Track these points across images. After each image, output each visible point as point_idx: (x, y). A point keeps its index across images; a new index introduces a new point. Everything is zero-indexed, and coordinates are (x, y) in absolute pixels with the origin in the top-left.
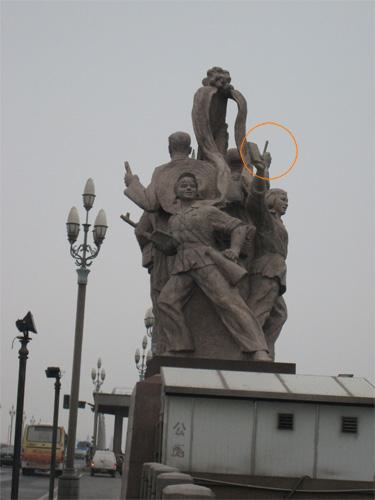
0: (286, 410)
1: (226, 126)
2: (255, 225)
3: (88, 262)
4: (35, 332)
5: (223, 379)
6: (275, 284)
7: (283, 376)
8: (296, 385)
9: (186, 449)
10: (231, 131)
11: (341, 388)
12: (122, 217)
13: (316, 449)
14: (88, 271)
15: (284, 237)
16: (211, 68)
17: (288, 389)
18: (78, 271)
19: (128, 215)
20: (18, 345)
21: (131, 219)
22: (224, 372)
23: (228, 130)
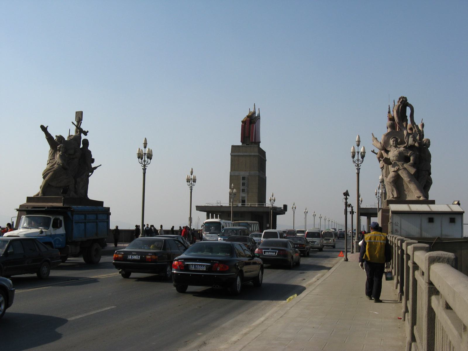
0: (430, 216)
1: (407, 116)
3: (359, 165)
4: (349, 196)
5: (410, 208)
7: (430, 205)
8: (434, 208)
9: (399, 230)
10: (409, 118)
12: (372, 151)
13: (441, 228)
15: (429, 156)
17: (431, 210)
18: (357, 168)
19: (374, 150)
20: (344, 201)
21: (375, 151)
22: (410, 205)
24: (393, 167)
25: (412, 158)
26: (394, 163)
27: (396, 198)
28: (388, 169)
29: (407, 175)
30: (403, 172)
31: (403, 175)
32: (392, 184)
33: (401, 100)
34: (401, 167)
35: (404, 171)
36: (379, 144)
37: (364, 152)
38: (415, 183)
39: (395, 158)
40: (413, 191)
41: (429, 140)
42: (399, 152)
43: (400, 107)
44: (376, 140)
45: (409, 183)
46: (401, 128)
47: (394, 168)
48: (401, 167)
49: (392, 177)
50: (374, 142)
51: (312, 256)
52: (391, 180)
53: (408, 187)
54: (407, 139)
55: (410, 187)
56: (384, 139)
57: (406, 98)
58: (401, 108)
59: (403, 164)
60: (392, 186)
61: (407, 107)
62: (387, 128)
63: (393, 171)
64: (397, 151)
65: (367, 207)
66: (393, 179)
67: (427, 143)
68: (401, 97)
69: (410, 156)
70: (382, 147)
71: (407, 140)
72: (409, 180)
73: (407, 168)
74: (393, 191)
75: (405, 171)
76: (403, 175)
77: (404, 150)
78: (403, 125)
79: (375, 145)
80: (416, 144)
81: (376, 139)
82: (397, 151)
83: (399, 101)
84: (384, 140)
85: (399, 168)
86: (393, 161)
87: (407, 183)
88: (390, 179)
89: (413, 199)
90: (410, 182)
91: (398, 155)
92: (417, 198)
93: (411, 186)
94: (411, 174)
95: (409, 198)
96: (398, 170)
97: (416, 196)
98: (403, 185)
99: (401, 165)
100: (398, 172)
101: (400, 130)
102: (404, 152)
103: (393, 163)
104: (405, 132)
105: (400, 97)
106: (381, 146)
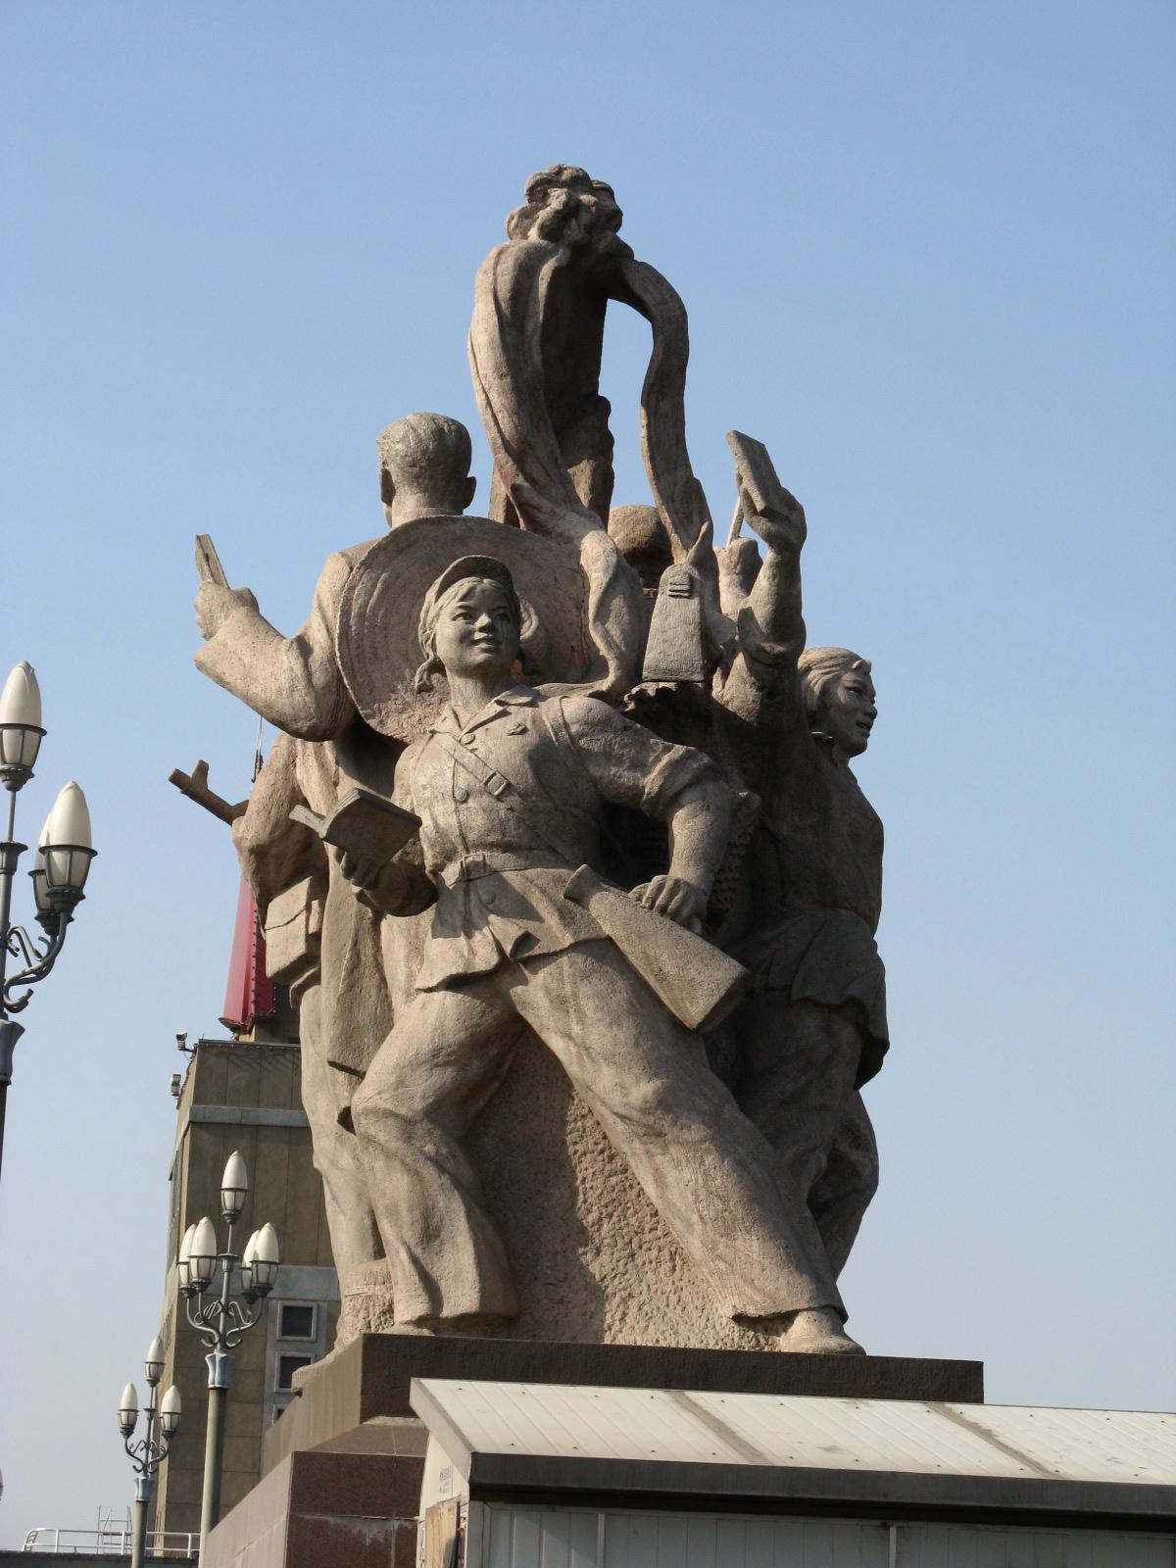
1: (604, 407)
2: (752, 787)
6: (847, 1034)
10: (628, 426)
11: (433, 1391)
12: (178, 779)
14: (16, 1031)
15: (869, 834)
16: (879, 704)
19: (203, 769)
21: (215, 785)
23: (614, 424)
24: (453, 933)
25: (685, 829)
26: (467, 875)
27: (463, 1321)
28: (369, 983)
29: (625, 1032)
30: (585, 989)
31: (576, 1029)
32: (429, 1148)
33: (557, 199)
34: (554, 932)
35: (586, 977)
36: (288, 662)
37: (81, 850)
38: (724, 1142)
39: (477, 817)
40: (695, 1245)
41: (864, 669)
42: (531, 738)
43: (547, 270)
44: (239, 614)
45: (654, 1134)
46: (545, 504)
47: (462, 940)
48: (554, 932)
49: (436, 1052)
50: (222, 634)
51: (597, 1544)
52: (424, 1087)
53: (631, 1184)
54: (614, 628)
55: (651, 1190)
56: (348, 601)
57: (606, 191)
58: (552, 286)
59: (578, 896)
60: (430, 1172)
61: (613, 305)
62: (388, 493)
63: (454, 983)
64: (509, 724)
65: (38, 1547)
66: (447, 1075)
67: (841, 694)
68: (560, 171)
69: (668, 800)
70: (318, 695)
71: (615, 632)
72: (644, 1090)
73: (624, 946)
74: (430, 1233)
75: (598, 984)
76: (576, 1029)
77: (594, 725)
78: (568, 484)
79: (233, 676)
80: (734, 689)
81: (248, 601)
82: (509, 724)
83: (527, 215)
84: (345, 613)
85: (525, 940)
86: (449, 856)
87: (618, 1130)
88: (400, 1083)
89: (694, 1343)
90: (666, 1124)
91: (524, 778)
92: (736, 1331)
93: (672, 1176)
94: (677, 1025)
95: (626, 1330)
96: (520, 958)
97: (725, 1310)
98: (560, 1168)
99: (553, 902)
100: (517, 991)
101: (531, 520)
102: (593, 744)
103: (451, 874)
104: (596, 555)
105: (546, 168)
106: (301, 685)
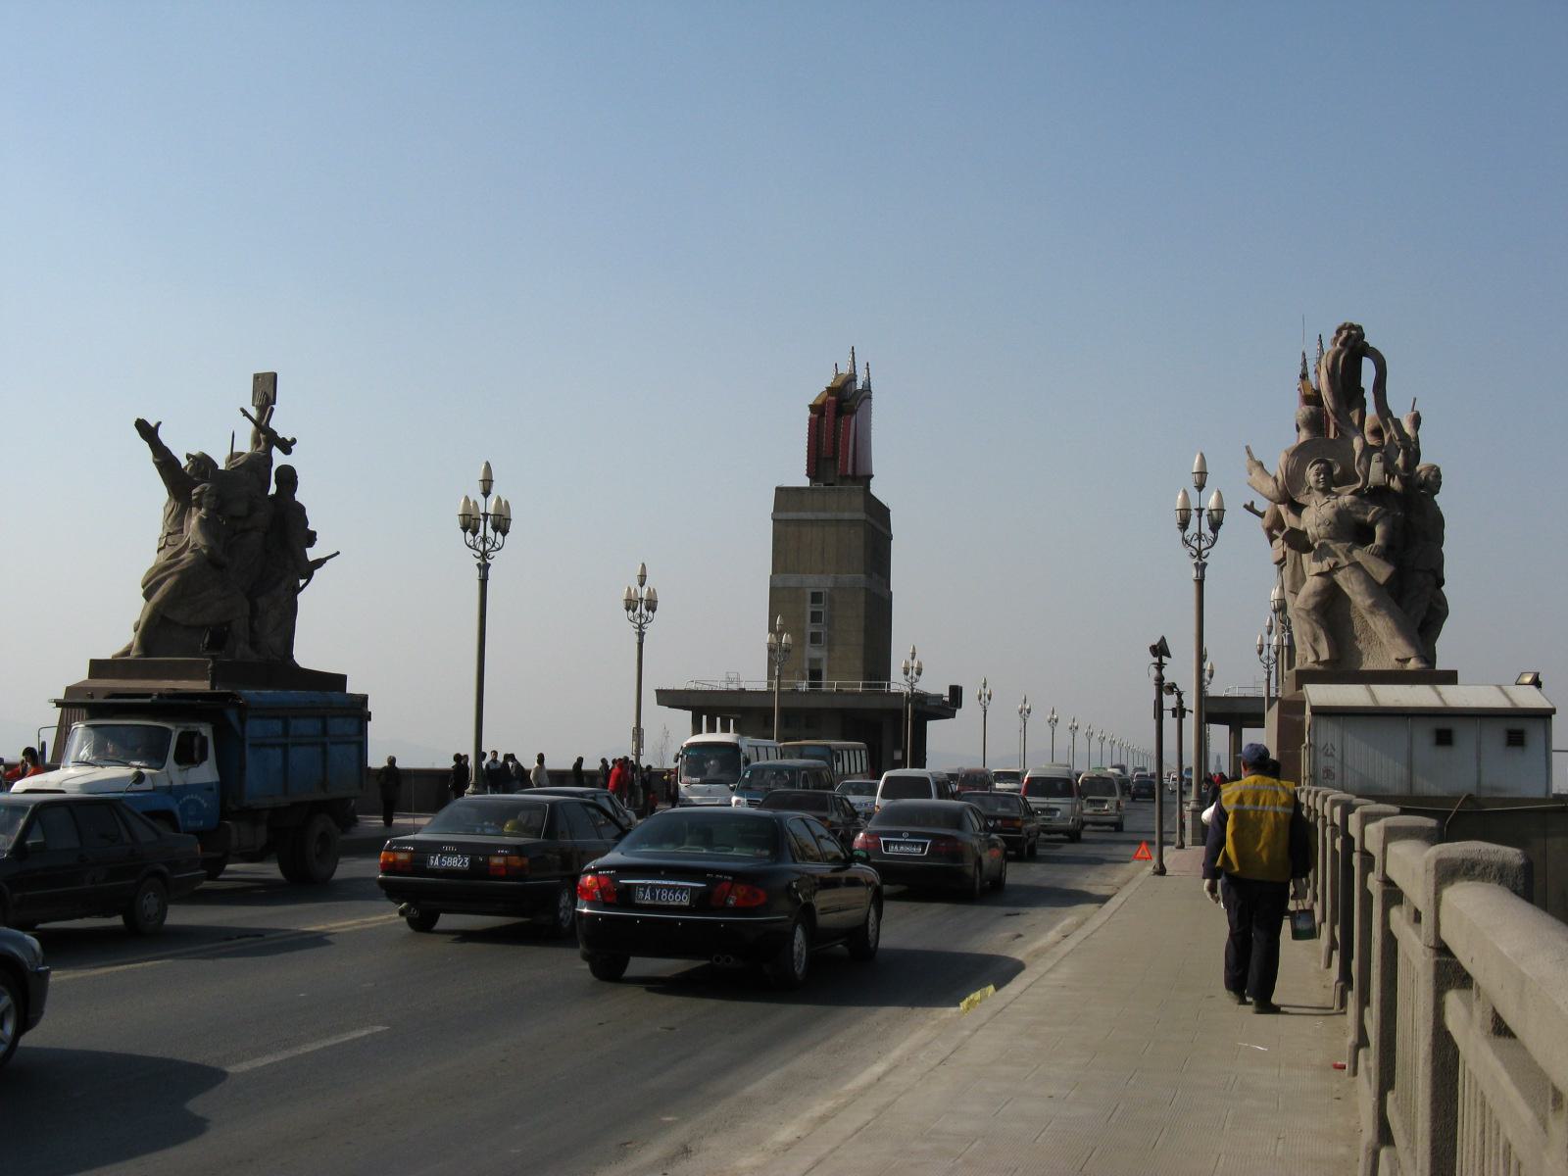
0: (1441, 724)
1: (1363, 390)
3: (1204, 553)
4: (1169, 656)
5: (1373, 695)
7: (1441, 688)
8: (1455, 696)
9: (1336, 771)
10: (1369, 396)
12: (1246, 506)
13: (1478, 765)
15: (1439, 521)
17: (1445, 703)
18: (1196, 564)
19: (1252, 503)
20: (1154, 672)
21: (1256, 507)
22: (1373, 687)
24: (1317, 561)
25: (1379, 530)
26: (1320, 545)
27: (1325, 662)
28: (1299, 567)
29: (1363, 587)
30: (1352, 576)
31: (1350, 586)
32: (1314, 618)
33: (1345, 333)
34: (1344, 561)
35: (1353, 572)
36: (1271, 483)
37: (1221, 510)
38: (1391, 614)
39: (1322, 531)
40: (1385, 641)
41: (1438, 470)
42: (1336, 509)
43: (1342, 357)
44: (1258, 469)
45: (1372, 613)
46: (1344, 428)
47: (1319, 563)
48: (1344, 561)
49: (1315, 592)
50: (1254, 475)
51: (1044, 856)
52: (1312, 602)
53: (1367, 625)
54: (1362, 467)
55: (1373, 627)
56: (1287, 466)
57: (1359, 328)
58: (1343, 362)
59: (1350, 551)
60: (1314, 624)
61: (1364, 358)
62: (1298, 430)
63: (1318, 574)
64: (1330, 505)
65: (1229, 694)
66: (1318, 599)
67: (1431, 478)
68: (1345, 324)
69: (1374, 522)
70: (1280, 493)
71: (1363, 469)
72: (1369, 602)
73: (1363, 564)
74: (1316, 639)
75: (1356, 575)
76: (1350, 586)
77: (1353, 503)
78: (1351, 420)
79: (1257, 487)
80: (1395, 484)
81: (1261, 465)
82: (1330, 505)
83: (1336, 339)
84: (1287, 469)
85: (1336, 564)
86: (1315, 540)
87: (1363, 612)
88: (1306, 601)
89: (1385, 668)
90: (1375, 610)
91: (1334, 520)
92: (1396, 663)
93: (1377, 623)
94: (1377, 583)
95: (1369, 664)
96: (1335, 568)
97: (1393, 657)
98: (1350, 621)
99: (1343, 553)
100: (1335, 576)
101: (1341, 434)
102: (1353, 509)
103: (1316, 545)
104: (1357, 443)
105: (1341, 324)
106: (1275, 490)
